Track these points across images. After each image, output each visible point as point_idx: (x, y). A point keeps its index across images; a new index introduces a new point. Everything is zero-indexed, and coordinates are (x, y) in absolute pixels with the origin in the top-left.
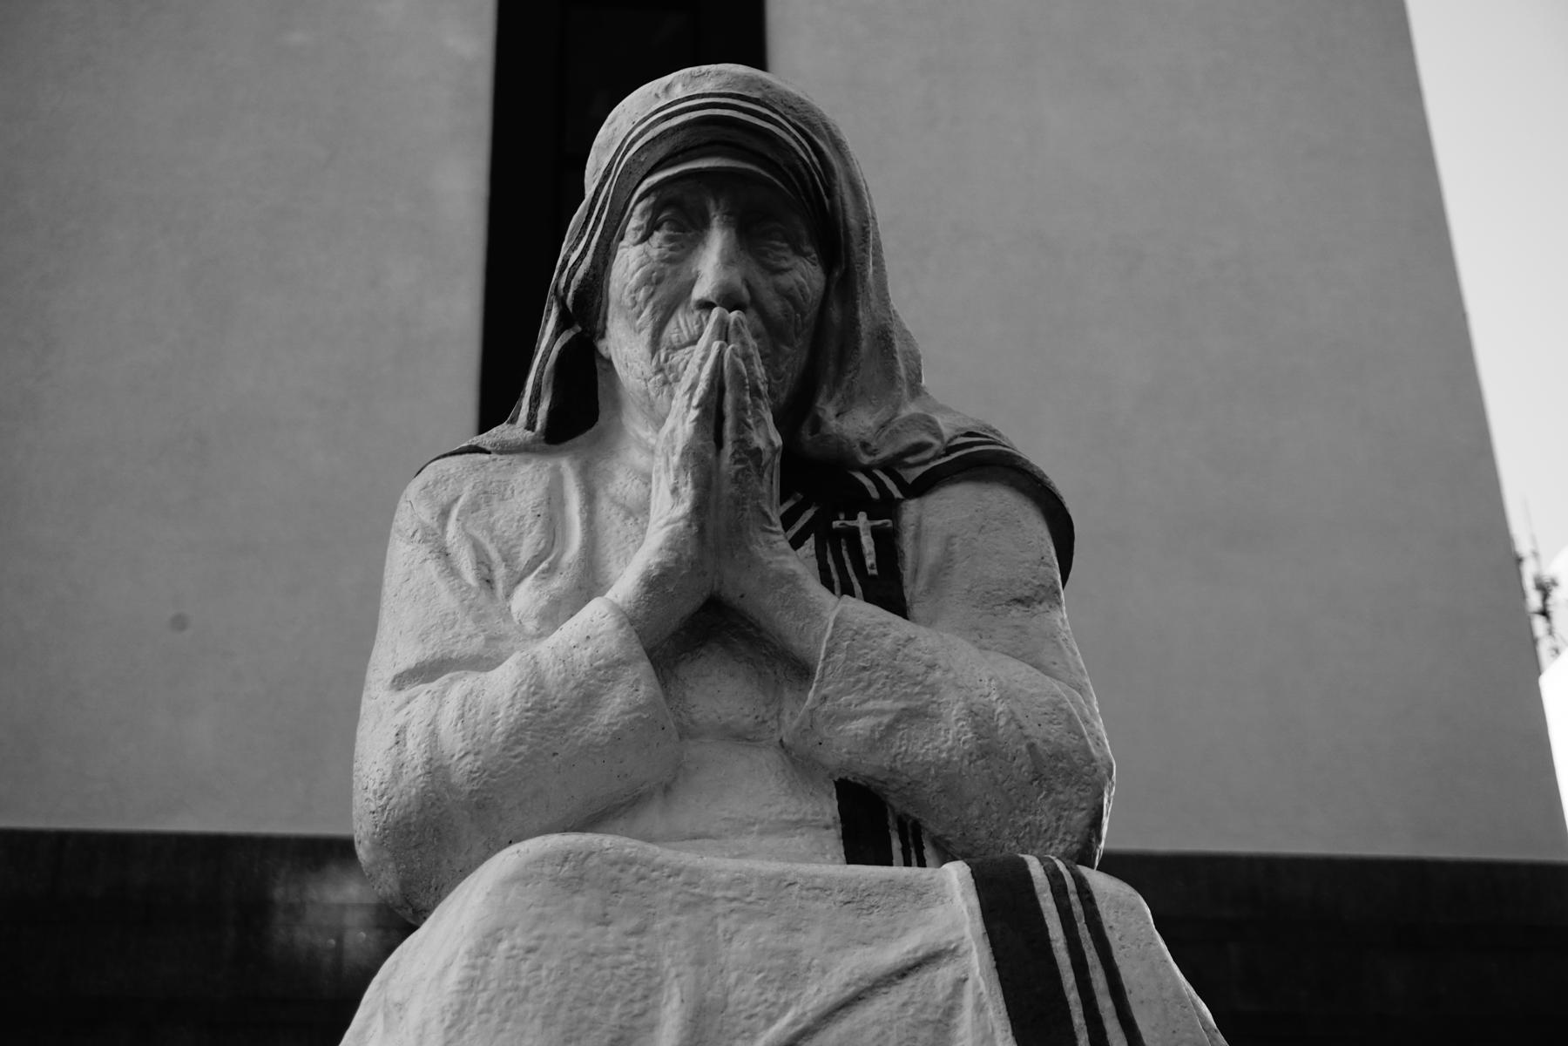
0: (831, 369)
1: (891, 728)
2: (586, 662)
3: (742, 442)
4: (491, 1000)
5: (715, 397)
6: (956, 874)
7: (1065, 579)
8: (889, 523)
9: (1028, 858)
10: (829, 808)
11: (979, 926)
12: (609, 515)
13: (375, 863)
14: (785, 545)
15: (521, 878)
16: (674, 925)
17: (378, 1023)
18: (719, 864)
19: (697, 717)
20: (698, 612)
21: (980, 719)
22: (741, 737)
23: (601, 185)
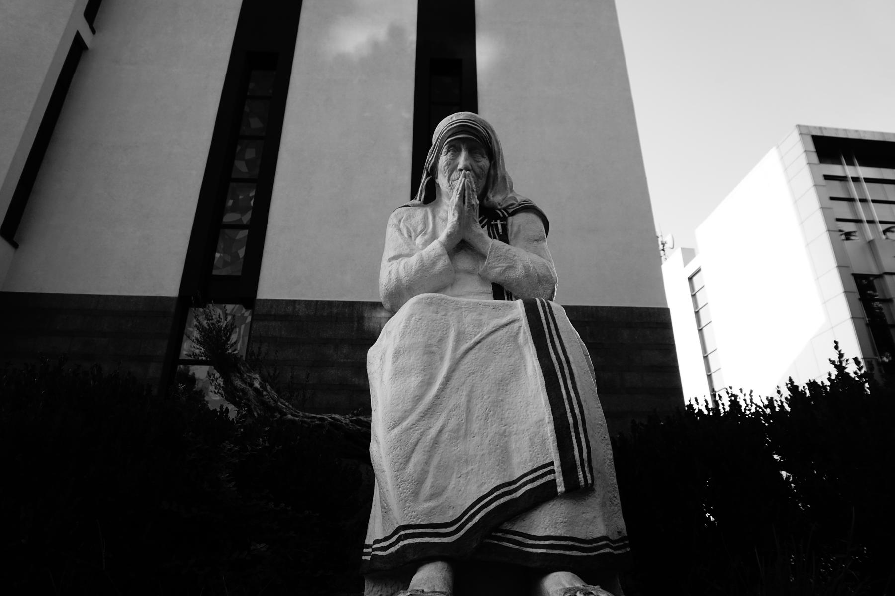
0: (491, 185)
1: (505, 270)
2: (433, 255)
3: (470, 203)
4: (411, 330)
5: (463, 191)
6: (519, 303)
7: (547, 236)
8: (505, 222)
9: (536, 299)
10: (490, 289)
11: (525, 314)
12: (439, 221)
13: (385, 302)
14: (480, 227)
15: (418, 303)
16: (453, 314)
17: (385, 336)
18: (464, 300)
19: (459, 268)
20: (459, 244)
21: (526, 268)
22: (469, 272)
23: (436, 142)
